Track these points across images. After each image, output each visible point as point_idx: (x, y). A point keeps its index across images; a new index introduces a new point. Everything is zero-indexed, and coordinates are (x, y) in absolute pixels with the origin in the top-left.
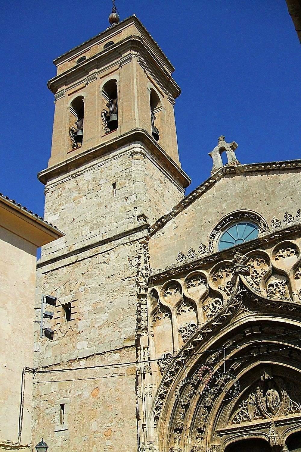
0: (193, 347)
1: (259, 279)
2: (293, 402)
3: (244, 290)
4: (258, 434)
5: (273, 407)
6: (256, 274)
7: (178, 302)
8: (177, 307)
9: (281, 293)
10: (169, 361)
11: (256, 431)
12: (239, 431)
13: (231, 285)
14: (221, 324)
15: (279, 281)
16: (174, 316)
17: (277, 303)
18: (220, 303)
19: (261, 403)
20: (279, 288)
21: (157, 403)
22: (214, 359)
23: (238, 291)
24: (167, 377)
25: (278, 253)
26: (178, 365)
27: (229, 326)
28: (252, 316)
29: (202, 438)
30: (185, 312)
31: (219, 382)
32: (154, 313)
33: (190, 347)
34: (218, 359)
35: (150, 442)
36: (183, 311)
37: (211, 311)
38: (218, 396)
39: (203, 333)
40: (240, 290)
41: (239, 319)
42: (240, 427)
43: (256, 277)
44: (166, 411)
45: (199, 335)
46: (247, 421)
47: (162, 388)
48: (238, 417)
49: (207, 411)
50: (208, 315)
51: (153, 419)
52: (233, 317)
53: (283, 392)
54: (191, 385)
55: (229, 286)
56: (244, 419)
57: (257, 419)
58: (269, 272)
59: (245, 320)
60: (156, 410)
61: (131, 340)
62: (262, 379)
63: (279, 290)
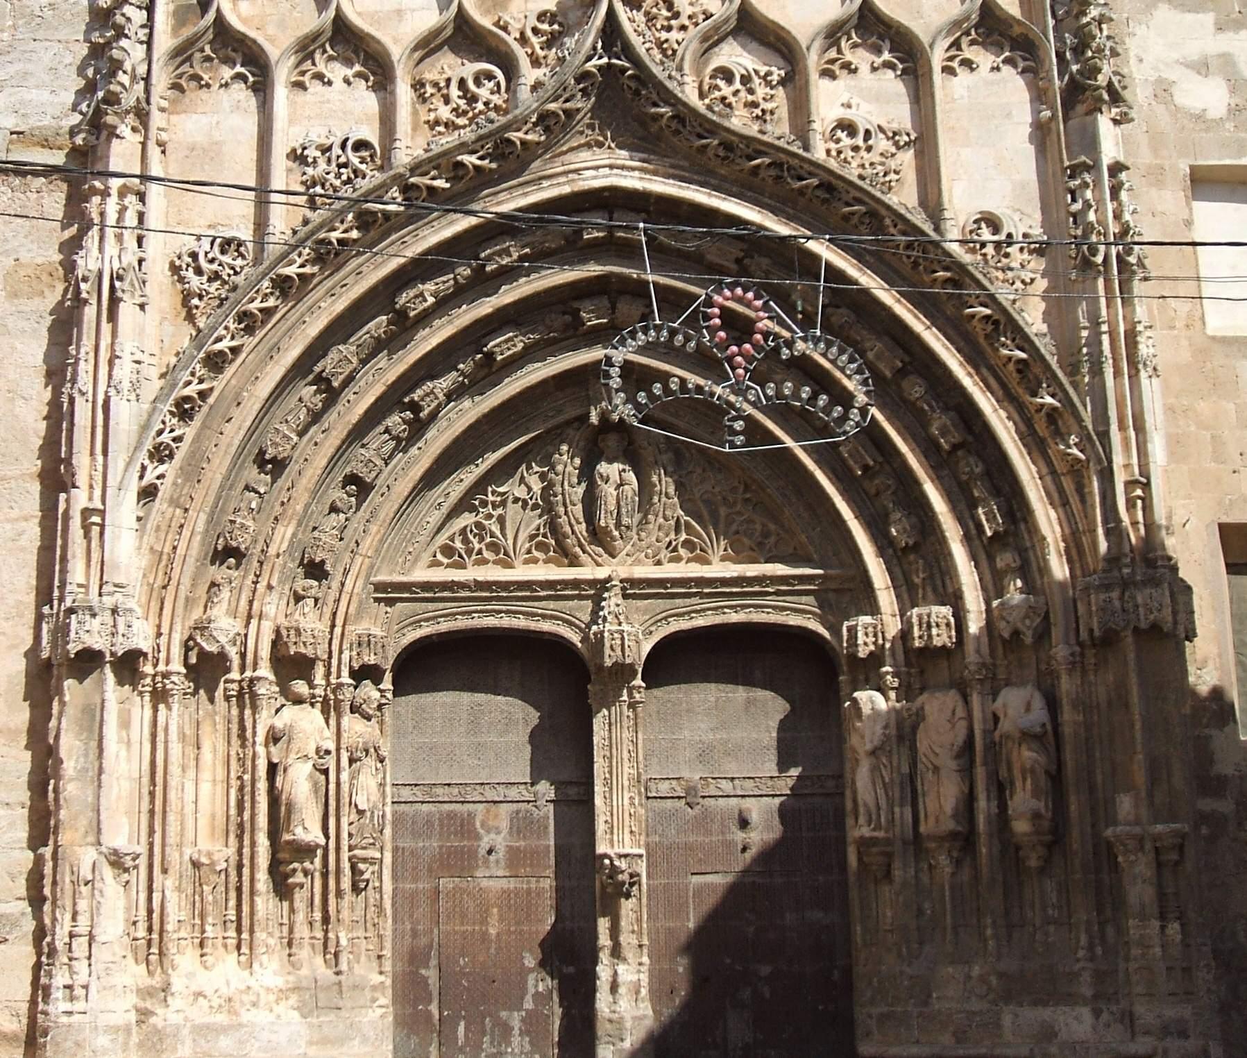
0: (355, 234)
1: (675, 35)
2: (687, 524)
3: (614, 61)
4: (544, 617)
5: (618, 525)
6: (669, 14)
7: (306, 37)
8: (296, 52)
9: (758, 112)
10: (233, 268)
11: (536, 604)
12: (468, 594)
13: (556, 27)
14: (491, 170)
15: (757, 68)
16: (281, 93)
17: (748, 147)
18: (498, 85)
19: (566, 507)
20: (751, 91)
21: (160, 433)
22: (431, 300)
23: (589, 59)
24: (224, 332)
25: (309, 62)
26: (277, 294)
27: (521, 185)
28: (623, 168)
29: (316, 600)
30: (330, 83)
31: (427, 395)
32: (182, 53)
33: (345, 231)
34: (444, 304)
35: (116, 585)
36: (319, 77)
37: (449, 108)
38: (405, 450)
39: (415, 187)
40: (600, 58)
41: (566, 168)
42: (479, 579)
43: (666, 23)
44: (193, 472)
45: (395, 192)
46: (495, 562)
47: (193, 374)
48: (458, 544)
49: (353, 499)
50: (437, 122)
51: (133, 496)
52: (541, 156)
53: (664, 483)
54: (311, 384)
55: (545, 27)
56: (486, 554)
57: (536, 561)
58: (727, 20)
59: (595, 178)
60: (151, 456)
61: (46, 144)
62: (594, 419)
63: (750, 98)
